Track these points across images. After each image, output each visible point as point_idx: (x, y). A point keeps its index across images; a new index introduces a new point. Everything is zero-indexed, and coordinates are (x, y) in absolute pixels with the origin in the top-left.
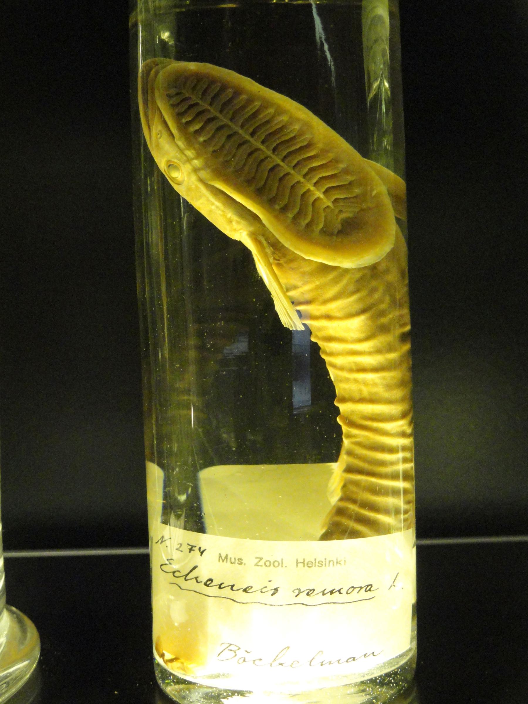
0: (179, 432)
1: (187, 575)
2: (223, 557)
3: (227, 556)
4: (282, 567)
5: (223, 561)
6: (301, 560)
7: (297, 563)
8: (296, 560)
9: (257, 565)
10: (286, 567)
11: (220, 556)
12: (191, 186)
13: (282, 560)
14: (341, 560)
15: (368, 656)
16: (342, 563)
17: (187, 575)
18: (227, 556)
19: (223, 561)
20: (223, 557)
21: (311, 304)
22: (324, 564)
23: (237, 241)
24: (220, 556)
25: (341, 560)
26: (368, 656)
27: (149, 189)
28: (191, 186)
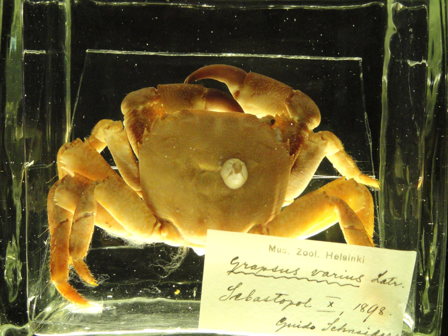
0: (14, 79)
1: (306, 303)
2: (273, 247)
3: (275, 247)
4: (315, 256)
5: (272, 250)
6: (330, 253)
7: (327, 255)
8: (326, 253)
9: (298, 254)
10: (318, 257)
11: (270, 247)
12: (280, 135)
13: (316, 252)
14: (361, 258)
15: (239, 300)
16: (362, 260)
17: (306, 303)
18: (275, 247)
19: (272, 250)
20: (273, 247)
21: (299, 171)
22: (347, 258)
23: (333, 166)
24: (270, 247)
25: (361, 258)
26: (239, 300)
27: (421, 179)
28: (280, 135)
